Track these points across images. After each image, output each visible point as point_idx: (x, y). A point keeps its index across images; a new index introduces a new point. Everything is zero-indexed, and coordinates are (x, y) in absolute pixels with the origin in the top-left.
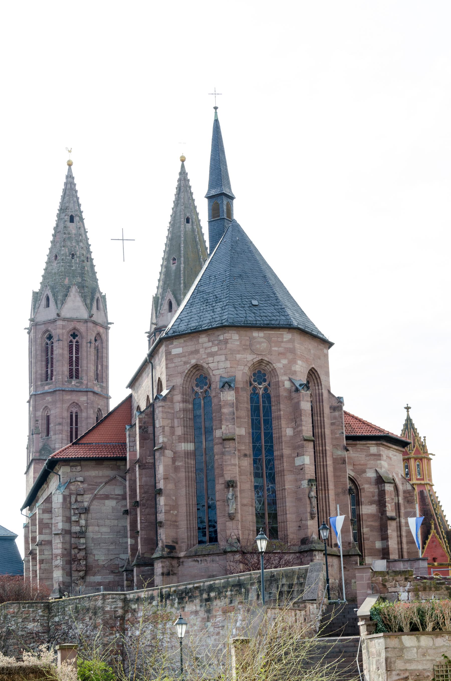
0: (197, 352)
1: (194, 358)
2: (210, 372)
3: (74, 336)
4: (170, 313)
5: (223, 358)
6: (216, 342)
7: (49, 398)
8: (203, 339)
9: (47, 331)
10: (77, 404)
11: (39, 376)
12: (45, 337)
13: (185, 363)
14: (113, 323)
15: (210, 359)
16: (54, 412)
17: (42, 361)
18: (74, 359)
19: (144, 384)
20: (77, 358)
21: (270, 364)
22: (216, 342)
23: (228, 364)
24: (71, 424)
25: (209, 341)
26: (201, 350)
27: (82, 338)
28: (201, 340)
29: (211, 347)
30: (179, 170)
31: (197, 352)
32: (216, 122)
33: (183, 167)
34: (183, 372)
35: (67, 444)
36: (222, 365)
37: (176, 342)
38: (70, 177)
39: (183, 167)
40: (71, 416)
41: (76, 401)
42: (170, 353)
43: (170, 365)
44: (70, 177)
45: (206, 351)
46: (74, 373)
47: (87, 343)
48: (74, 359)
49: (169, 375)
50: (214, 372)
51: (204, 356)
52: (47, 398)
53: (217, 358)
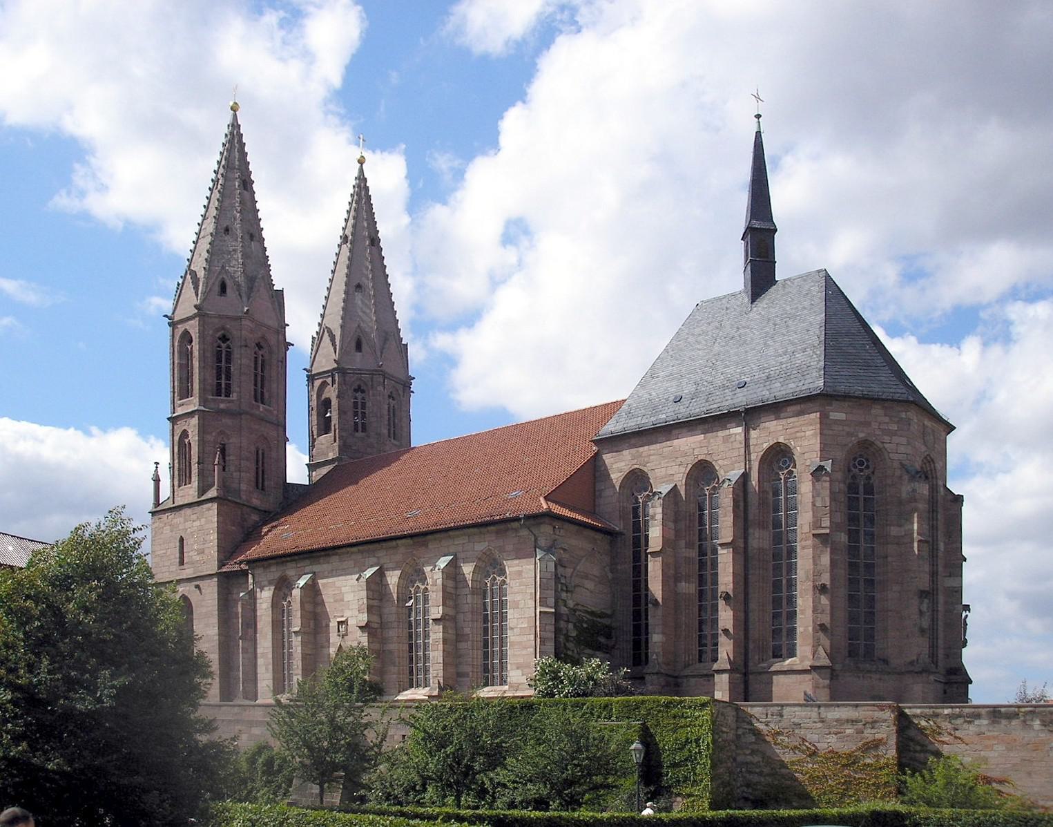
0: (868, 424)
1: (862, 432)
2: (886, 454)
4: (359, 354)
5: (904, 440)
6: (896, 419)
7: (227, 421)
8: (877, 410)
9: (223, 328)
10: (266, 438)
11: (209, 387)
13: (849, 434)
14: (293, 345)
15: (887, 439)
16: (233, 441)
17: (213, 368)
18: (223, 376)
19: (676, 442)
20: (219, 378)
22: (896, 419)
23: (909, 450)
24: (257, 461)
25: (885, 415)
26: (873, 424)
27: (271, 352)
28: (873, 411)
30: (356, 174)
31: (868, 424)
32: (758, 135)
33: (361, 170)
34: (845, 445)
35: (792, 498)
36: (902, 449)
37: (835, 404)
38: (235, 126)
39: (361, 170)
41: (265, 434)
42: (828, 417)
43: (825, 432)
44: (235, 126)
46: (259, 397)
48: (223, 376)
49: (825, 444)
50: (891, 455)
52: (223, 420)
53: (896, 439)
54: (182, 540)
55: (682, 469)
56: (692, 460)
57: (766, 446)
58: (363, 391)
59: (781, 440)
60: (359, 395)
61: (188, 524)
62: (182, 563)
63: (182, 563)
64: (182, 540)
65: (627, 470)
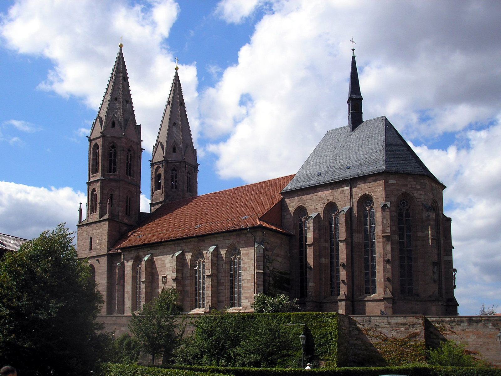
3: (129, 150)
4: (174, 154)
5: (423, 193)
7: (113, 184)
8: (410, 179)
9: (113, 142)
12: (110, 146)
13: (398, 190)
15: (415, 192)
19: (319, 194)
21: (436, 203)
28: (409, 179)
29: (415, 185)
31: (407, 185)
32: (353, 58)
33: (177, 73)
36: (422, 197)
38: (121, 54)
39: (177, 73)
40: (127, 199)
43: (387, 189)
44: (121, 54)
45: (412, 187)
47: (137, 157)
51: (411, 189)
52: (112, 184)
53: (419, 192)
54: (91, 238)
55: (322, 206)
56: (326, 202)
57: (360, 195)
58: (176, 171)
59: (367, 192)
60: (174, 172)
61: (94, 231)
62: (91, 249)
63: (91, 249)
64: (91, 238)
65: (296, 206)
